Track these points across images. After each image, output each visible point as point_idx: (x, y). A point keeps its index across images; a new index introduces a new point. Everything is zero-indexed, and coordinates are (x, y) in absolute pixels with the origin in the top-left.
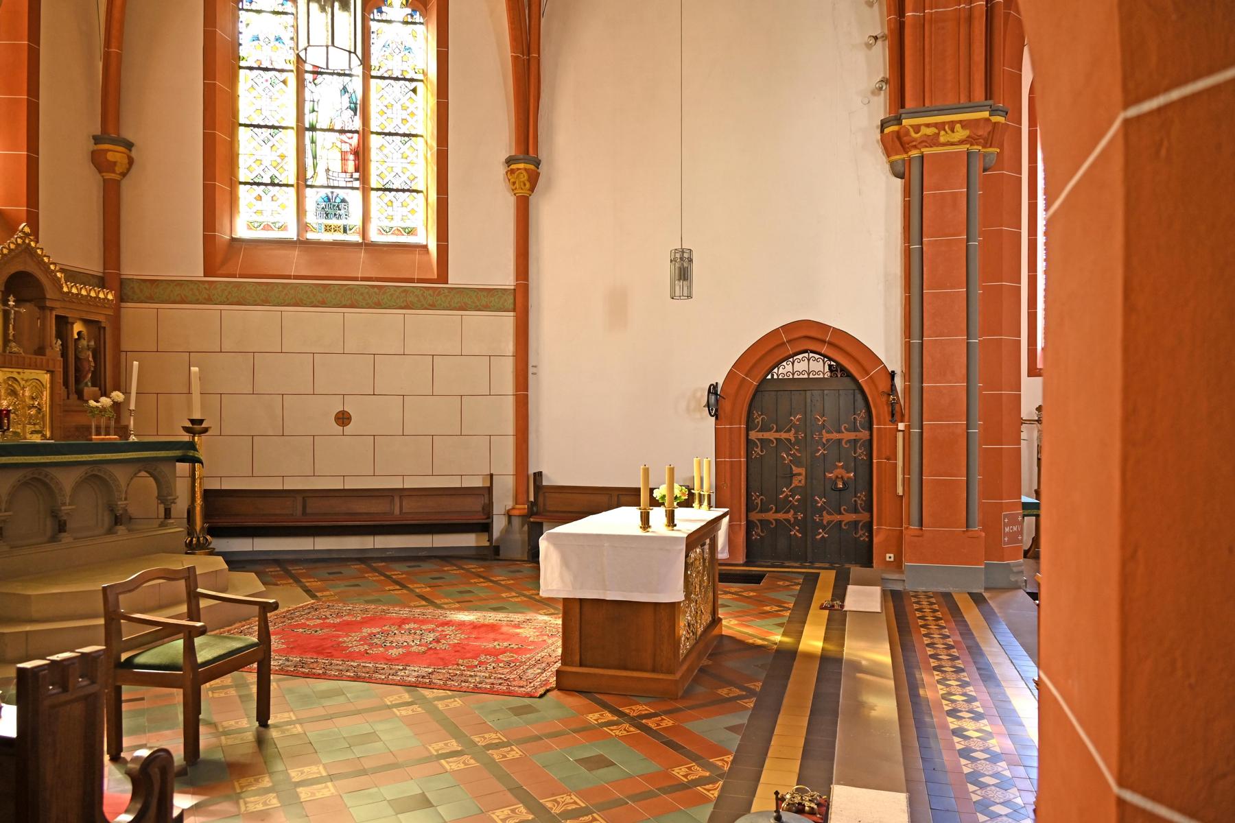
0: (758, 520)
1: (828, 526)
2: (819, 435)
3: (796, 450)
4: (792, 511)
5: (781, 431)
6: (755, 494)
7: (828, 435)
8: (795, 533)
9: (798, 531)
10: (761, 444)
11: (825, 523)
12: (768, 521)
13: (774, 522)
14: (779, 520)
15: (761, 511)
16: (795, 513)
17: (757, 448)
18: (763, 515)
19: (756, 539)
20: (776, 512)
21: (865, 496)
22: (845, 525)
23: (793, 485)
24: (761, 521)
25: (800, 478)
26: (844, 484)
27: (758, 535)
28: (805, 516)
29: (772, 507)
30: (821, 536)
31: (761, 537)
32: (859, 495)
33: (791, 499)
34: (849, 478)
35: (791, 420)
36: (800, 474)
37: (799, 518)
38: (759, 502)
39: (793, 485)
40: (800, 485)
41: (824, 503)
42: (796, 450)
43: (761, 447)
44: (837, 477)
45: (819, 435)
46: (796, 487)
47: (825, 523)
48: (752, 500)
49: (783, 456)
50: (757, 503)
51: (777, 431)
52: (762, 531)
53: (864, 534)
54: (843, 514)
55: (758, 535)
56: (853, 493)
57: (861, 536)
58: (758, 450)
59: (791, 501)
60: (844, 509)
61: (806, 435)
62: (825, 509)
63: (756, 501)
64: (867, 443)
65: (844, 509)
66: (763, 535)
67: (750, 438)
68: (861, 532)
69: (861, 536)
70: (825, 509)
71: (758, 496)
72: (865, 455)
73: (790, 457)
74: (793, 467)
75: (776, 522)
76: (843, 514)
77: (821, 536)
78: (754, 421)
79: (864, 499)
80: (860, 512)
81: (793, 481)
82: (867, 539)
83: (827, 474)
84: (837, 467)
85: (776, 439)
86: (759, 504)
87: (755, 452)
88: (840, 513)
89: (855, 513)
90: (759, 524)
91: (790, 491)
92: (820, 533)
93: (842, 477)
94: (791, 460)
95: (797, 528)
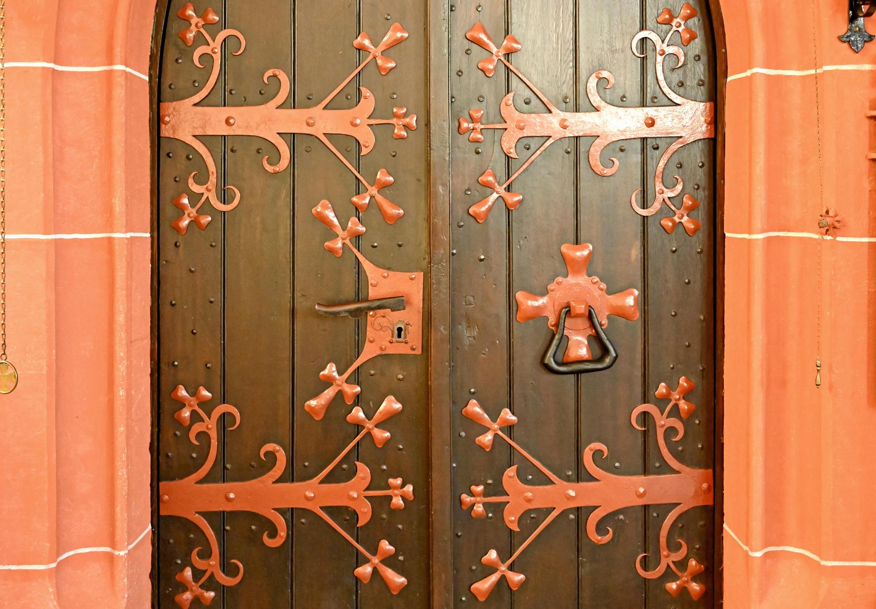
0: (208, 515)
1: (524, 535)
2: (485, 494)
3: (383, 187)
4: (364, 471)
5: (310, 101)
6: (194, 393)
7: (529, 492)
8: (375, 570)
9: (389, 561)
10: (222, 534)
11: (511, 519)
12: (253, 516)
13: (280, 522)
14: (305, 512)
15: (220, 474)
16: (378, 481)
17: (201, 179)
18: (239, 114)
19: (197, 600)
20: (290, 475)
21: (687, 395)
22: (600, 528)
23: (369, 352)
24: (218, 519)
25: (397, 318)
26: (596, 339)
27: (211, 584)
28: (424, 494)
29: (271, 456)
30: (493, 578)
31: (221, 590)
32: (662, 388)
33: (358, 413)
34: (618, 313)
35: (360, 49)
36: (398, 303)
37: (398, 502)
38: (214, 434)
39: (369, 352)
40: (401, 349)
41: (509, 429)
42: (383, 187)
43: (223, 176)
44: (568, 311)
45: (485, 494)
46: (385, 357)
47: (511, 519)
48: (178, 423)
49: (323, 220)
50: (203, 436)
51: (292, 103)
52: (228, 569)
53: (682, 565)
54: (592, 479)
55: (211, 584)
56: (638, 390)
57: (669, 575)
58: (208, 192)
59: (358, 427)
60: (597, 454)
61: (424, 494)
62: (511, 457)
63: (197, 428)
64: (698, 157)
65: (597, 454)
66: (229, 581)
67: (166, 132)
68: (668, 558)
69: (669, 575)
70: (511, 457)
71: (207, 406)
72: (690, 210)
73: (353, 224)
74: (367, 265)
75: (291, 526)
76: (592, 479)
77: (493, 578)
78: (187, 51)
79: (683, 405)
80: (664, 468)
81: (370, 333)
82: (695, 587)
83: (519, 295)
84: (567, 265)
85: (292, 139)
86: (214, 443)
87: (195, 198)
88: (580, 475)
89: (645, 472)
90: (210, 533)
91: (356, 378)
92: (490, 569)
93: (590, 317)
94: (357, 238)
95: (386, 546)
